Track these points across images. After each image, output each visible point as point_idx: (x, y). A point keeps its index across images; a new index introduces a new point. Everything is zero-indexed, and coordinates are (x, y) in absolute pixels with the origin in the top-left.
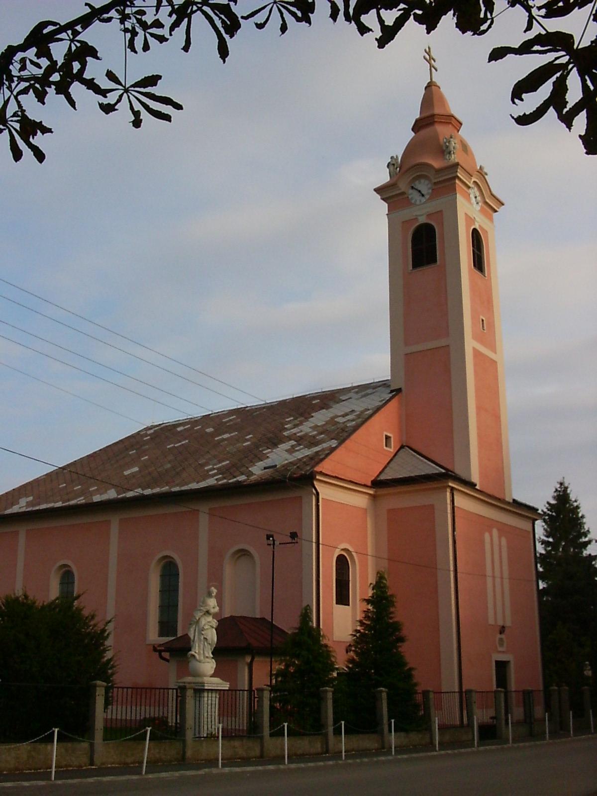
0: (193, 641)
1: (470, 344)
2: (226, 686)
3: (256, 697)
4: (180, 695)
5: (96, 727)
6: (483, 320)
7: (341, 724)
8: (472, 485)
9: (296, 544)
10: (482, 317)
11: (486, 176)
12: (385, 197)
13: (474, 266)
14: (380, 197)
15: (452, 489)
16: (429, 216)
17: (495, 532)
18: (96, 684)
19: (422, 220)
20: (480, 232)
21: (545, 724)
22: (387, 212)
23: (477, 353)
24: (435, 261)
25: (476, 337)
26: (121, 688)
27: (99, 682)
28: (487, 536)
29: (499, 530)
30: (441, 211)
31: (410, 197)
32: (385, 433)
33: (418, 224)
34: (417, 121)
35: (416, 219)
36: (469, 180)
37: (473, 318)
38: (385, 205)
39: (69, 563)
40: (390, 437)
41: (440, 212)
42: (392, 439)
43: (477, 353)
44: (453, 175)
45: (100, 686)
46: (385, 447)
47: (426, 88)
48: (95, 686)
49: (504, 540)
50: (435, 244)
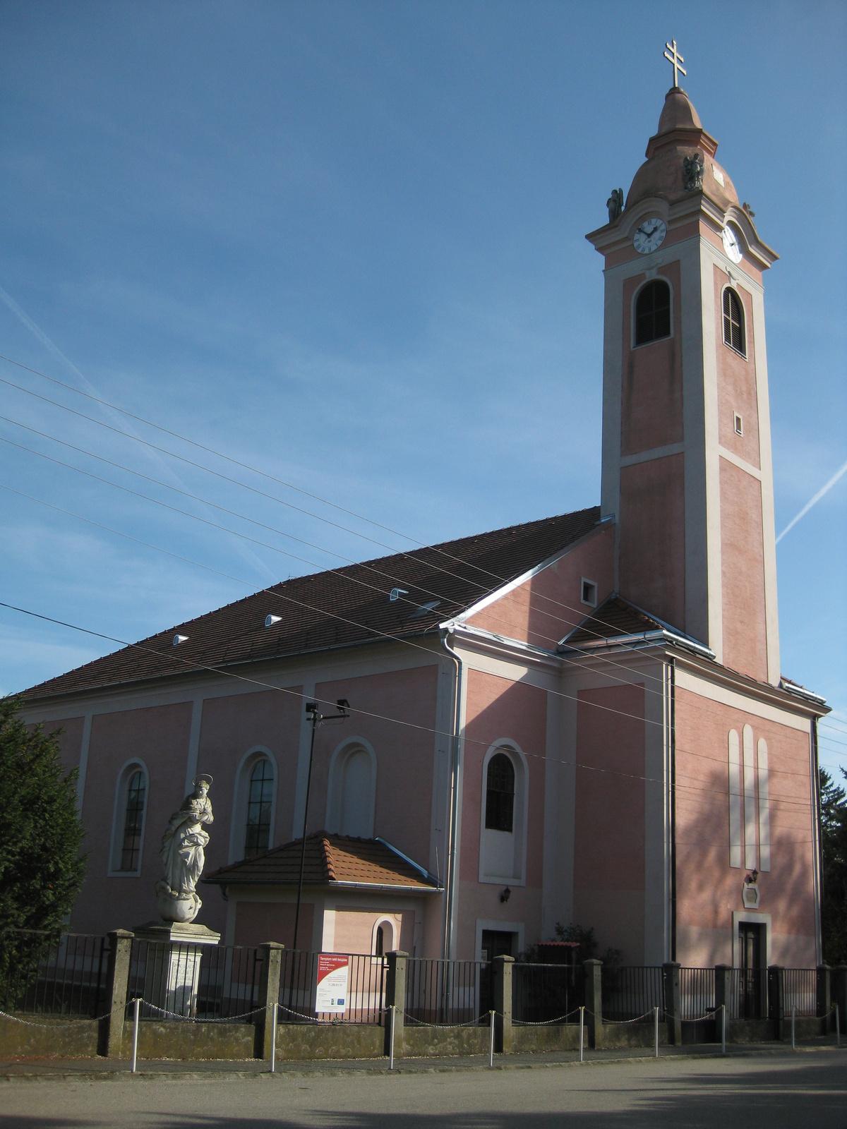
0: (166, 864)
1: (715, 452)
2: (214, 940)
3: (107, 950)
4: (109, 948)
5: (114, 998)
6: (738, 419)
7: (579, 1012)
8: (709, 659)
9: (347, 718)
10: (736, 414)
11: (751, 219)
12: (600, 245)
13: (727, 338)
14: (594, 247)
15: (671, 660)
16: (662, 270)
17: (748, 731)
18: (270, 945)
19: (652, 275)
20: (738, 293)
21: (654, 1026)
22: (604, 269)
23: (725, 465)
24: (667, 333)
25: (722, 440)
26: (363, 955)
27: (506, 957)
28: (734, 735)
29: (755, 728)
30: (679, 261)
31: (635, 245)
32: (584, 580)
33: (644, 282)
34: (652, 140)
35: (642, 276)
36: (721, 218)
37: (721, 413)
38: (600, 259)
39: (142, 763)
40: (592, 587)
41: (677, 263)
42: (596, 589)
43: (725, 465)
44: (696, 209)
45: (123, 937)
46: (583, 601)
47: (667, 96)
48: (268, 948)
49: (762, 743)
50: (668, 311)
